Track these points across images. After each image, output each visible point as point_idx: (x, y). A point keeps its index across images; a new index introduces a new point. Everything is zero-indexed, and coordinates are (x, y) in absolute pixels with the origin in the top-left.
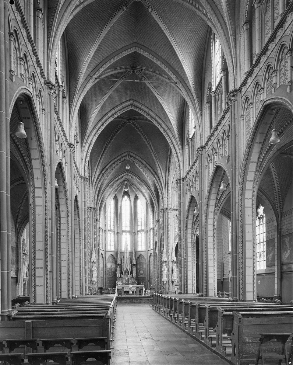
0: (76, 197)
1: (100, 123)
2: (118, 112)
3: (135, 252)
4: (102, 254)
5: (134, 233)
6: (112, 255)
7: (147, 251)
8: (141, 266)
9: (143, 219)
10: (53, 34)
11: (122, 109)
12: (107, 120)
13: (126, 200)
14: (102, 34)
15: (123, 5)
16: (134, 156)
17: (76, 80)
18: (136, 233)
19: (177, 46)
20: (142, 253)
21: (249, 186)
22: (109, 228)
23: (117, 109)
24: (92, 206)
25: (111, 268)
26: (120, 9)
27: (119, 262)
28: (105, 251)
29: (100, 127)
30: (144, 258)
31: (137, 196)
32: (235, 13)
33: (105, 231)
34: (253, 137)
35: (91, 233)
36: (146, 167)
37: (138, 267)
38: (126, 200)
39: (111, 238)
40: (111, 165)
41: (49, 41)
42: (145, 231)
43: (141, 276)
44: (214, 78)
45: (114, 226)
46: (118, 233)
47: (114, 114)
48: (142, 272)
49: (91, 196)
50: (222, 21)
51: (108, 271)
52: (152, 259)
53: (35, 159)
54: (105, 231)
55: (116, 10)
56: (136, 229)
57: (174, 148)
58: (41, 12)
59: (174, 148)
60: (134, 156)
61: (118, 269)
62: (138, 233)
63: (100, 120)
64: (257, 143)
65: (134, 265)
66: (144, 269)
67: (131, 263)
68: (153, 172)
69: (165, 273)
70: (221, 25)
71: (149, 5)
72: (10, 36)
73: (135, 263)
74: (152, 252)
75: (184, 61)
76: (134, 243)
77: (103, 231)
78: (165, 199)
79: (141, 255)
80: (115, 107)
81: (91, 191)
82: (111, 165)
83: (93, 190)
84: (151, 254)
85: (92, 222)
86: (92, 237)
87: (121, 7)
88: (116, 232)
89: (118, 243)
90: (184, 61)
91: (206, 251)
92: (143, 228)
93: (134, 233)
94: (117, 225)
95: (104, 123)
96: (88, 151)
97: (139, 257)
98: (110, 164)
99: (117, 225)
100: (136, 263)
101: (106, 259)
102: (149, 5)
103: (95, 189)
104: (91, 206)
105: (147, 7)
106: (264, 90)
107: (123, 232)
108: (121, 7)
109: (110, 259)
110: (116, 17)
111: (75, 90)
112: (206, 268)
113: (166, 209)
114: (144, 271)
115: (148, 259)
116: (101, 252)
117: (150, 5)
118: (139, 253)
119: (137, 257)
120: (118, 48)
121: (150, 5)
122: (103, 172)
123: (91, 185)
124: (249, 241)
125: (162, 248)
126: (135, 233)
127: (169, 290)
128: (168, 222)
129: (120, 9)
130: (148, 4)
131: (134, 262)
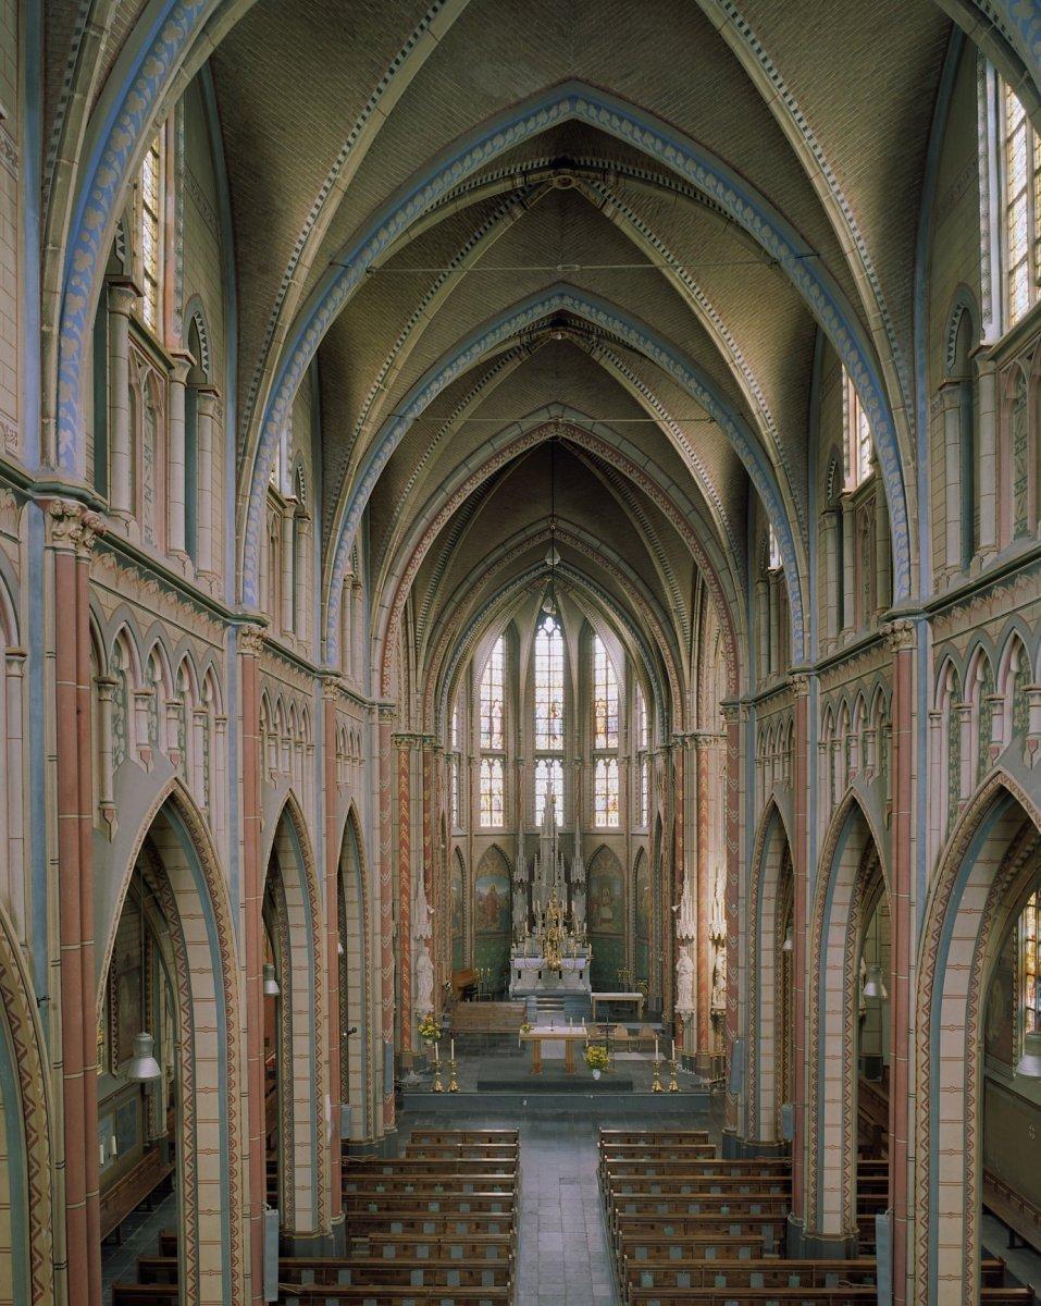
0: (351, 815)
1: (442, 497)
2: (504, 450)
3: (584, 835)
4: (457, 850)
5: (579, 760)
6: (494, 846)
7: (626, 833)
8: (605, 891)
9: (613, 709)
10: (261, 411)
11: (519, 440)
12: (465, 483)
13: (550, 635)
14: (431, 304)
15: (512, 202)
16: (576, 531)
17: (348, 444)
18: (587, 757)
19: (713, 312)
20: (609, 841)
21: (955, 983)
22: (484, 743)
23: (499, 443)
24: (417, 728)
25: (492, 897)
26: (501, 213)
27: (520, 875)
28: (473, 833)
29: (440, 512)
30: (616, 860)
31: (589, 624)
32: (912, 316)
33: (470, 759)
34: (965, 841)
35: (413, 830)
36: (620, 571)
37: (595, 891)
38: (550, 635)
39: (491, 778)
40: (488, 570)
41: (242, 467)
42: (622, 754)
43: (605, 928)
44: (852, 415)
45: (503, 733)
46: (517, 762)
47: (490, 460)
48: (607, 913)
49: (413, 690)
50: (866, 346)
51: (482, 909)
52: (646, 872)
53: (191, 916)
54: (470, 759)
55: (488, 216)
56: (587, 747)
57: (716, 579)
58: (213, 395)
59: (716, 579)
60: (576, 531)
61: (519, 898)
62: (594, 765)
63: (440, 487)
64: (982, 862)
65: (578, 884)
66: (615, 903)
67: (567, 879)
68: (646, 594)
69: (687, 982)
70: (861, 358)
71: (606, 194)
72: (99, 688)
73: (582, 879)
74: (646, 843)
75: (741, 360)
76: (580, 796)
77: (464, 762)
78: (691, 698)
79: (604, 846)
80: (493, 437)
81: (412, 674)
82: (488, 570)
83: (421, 667)
84: (642, 849)
85: (418, 789)
86: (417, 819)
87: (503, 209)
88: (511, 757)
89: (518, 796)
90: (741, 360)
91: (817, 1065)
92: (614, 743)
93: (579, 760)
94: (517, 730)
95: (453, 496)
96: (394, 602)
97: (598, 855)
98: (482, 567)
99: (517, 730)
100: (588, 878)
101: (475, 869)
102: (606, 194)
103: (429, 660)
104: (413, 732)
105: (599, 203)
106: (1002, 704)
107: (537, 757)
108: (503, 209)
109: (489, 863)
110: (486, 239)
111: (344, 476)
112: (816, 1174)
113: (695, 737)
114: (614, 910)
115: (632, 867)
116: (455, 842)
117: (609, 196)
118: (600, 841)
119: (590, 852)
120: (498, 307)
121: (609, 196)
122: (457, 598)
123: (412, 651)
124: (951, 1184)
125: (678, 887)
126: (582, 760)
127: (699, 1047)
128: (699, 786)
129: (501, 213)
130: (604, 192)
131: (578, 873)
